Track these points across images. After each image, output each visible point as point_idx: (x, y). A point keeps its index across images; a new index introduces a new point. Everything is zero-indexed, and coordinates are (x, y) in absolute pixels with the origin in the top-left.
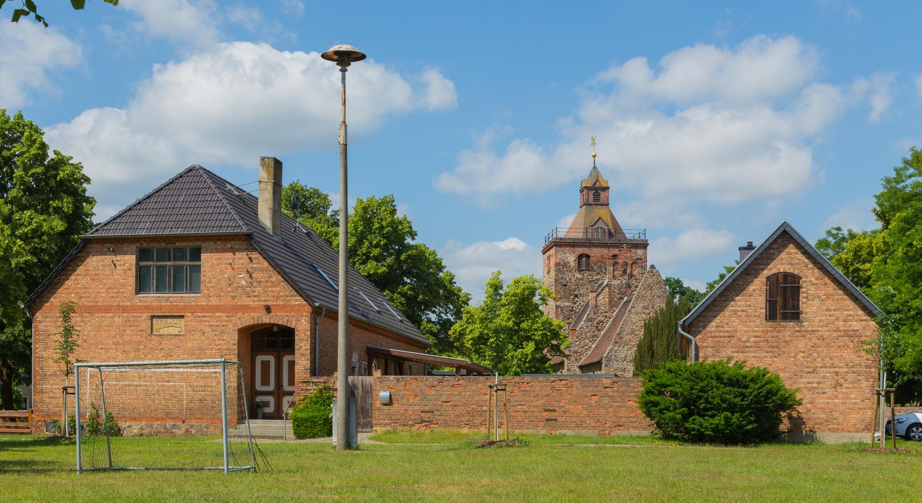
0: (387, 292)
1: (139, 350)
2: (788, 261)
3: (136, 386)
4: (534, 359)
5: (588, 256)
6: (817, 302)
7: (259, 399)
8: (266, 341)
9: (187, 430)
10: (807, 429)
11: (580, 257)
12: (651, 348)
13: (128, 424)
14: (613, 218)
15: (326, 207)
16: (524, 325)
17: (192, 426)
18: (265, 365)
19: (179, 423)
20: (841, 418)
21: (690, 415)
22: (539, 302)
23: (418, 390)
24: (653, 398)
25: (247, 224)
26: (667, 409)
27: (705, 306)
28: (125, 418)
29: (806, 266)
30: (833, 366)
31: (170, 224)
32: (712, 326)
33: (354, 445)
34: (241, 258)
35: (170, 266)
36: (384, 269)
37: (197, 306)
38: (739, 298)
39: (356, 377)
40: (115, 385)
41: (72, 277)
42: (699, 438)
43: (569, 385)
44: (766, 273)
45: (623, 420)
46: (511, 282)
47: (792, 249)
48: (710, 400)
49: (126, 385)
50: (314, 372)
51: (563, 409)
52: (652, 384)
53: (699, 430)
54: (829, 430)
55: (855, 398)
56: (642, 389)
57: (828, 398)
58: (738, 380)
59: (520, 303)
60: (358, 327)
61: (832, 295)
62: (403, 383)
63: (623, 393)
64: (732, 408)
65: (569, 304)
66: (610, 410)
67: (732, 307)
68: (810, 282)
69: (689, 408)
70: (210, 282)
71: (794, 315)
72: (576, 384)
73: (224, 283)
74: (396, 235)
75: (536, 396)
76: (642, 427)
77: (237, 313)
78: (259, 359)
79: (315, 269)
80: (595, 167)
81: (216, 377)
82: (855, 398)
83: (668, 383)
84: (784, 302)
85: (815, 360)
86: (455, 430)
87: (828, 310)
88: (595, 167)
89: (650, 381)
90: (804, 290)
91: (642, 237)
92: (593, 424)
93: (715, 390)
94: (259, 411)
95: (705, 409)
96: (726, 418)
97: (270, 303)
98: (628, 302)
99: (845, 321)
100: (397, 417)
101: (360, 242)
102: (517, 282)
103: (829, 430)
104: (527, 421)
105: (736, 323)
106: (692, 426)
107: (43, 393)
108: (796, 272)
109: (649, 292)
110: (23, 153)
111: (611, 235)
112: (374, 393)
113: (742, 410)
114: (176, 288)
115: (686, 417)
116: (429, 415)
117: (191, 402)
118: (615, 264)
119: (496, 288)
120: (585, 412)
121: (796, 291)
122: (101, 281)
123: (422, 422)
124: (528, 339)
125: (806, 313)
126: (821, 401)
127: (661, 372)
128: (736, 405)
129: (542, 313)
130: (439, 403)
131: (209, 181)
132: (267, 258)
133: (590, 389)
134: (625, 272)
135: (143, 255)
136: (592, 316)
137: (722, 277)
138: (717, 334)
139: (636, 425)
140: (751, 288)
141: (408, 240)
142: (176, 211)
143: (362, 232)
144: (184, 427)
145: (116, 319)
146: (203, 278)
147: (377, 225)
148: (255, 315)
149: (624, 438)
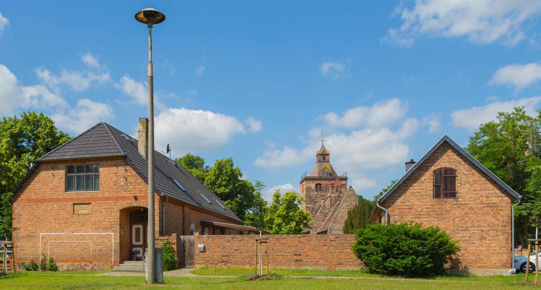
1: (67, 223)
2: (448, 160)
3: (66, 243)
4: (295, 230)
5: (320, 184)
6: (467, 186)
7: (134, 249)
8: (135, 216)
9: (92, 267)
10: (463, 266)
11: (317, 185)
12: (351, 223)
13: (61, 264)
14: (331, 167)
15: (202, 164)
16: (291, 214)
17: (95, 265)
18: (138, 230)
19: (88, 264)
20: (486, 259)
21: (388, 257)
22: (298, 203)
23: (220, 243)
24: (362, 247)
25: (124, 151)
26: (372, 254)
27: (394, 190)
28: (60, 261)
29: (460, 163)
30: (479, 226)
31: (83, 152)
32: (398, 202)
33: (160, 280)
34: (121, 170)
35: (83, 176)
36: (228, 190)
37: (98, 197)
38: (415, 184)
39: (185, 236)
40: (55, 243)
41: (32, 183)
42: (393, 273)
43: (309, 239)
44: (433, 168)
45: (342, 260)
46: (284, 194)
47: (450, 153)
48: (401, 248)
49: (60, 242)
50: (161, 234)
51: (306, 254)
52: (361, 238)
53: (394, 267)
54: (478, 267)
55: (495, 247)
56: (356, 241)
57: (476, 246)
58: (419, 235)
59: (289, 204)
60: (194, 210)
61: (478, 181)
62: (211, 239)
63: (343, 244)
64: (417, 253)
66: (335, 254)
67: (411, 190)
68: (463, 173)
69: (387, 253)
70: (104, 184)
71: (453, 194)
72: (313, 239)
73: (112, 184)
74: (233, 176)
75: (290, 246)
76: (356, 265)
77: (119, 201)
78: (134, 227)
79: (171, 179)
81: (108, 237)
82: (495, 247)
83: (373, 237)
84: (445, 186)
85: (467, 222)
86: (241, 267)
87: (475, 190)
89: (360, 236)
90: (458, 178)
91: (345, 176)
92: (324, 263)
93: (404, 241)
94: (134, 256)
95: (397, 254)
96: (412, 260)
97: (137, 195)
98: (339, 204)
99: (487, 197)
100: (208, 259)
101: (217, 179)
102: (287, 194)
103: (478, 267)
104: (284, 261)
105: (414, 200)
106: (390, 265)
107: (17, 247)
108: (453, 167)
109: (349, 198)
110: (42, 132)
111: (330, 175)
112: (195, 245)
113: (423, 254)
114: (87, 188)
115: (385, 259)
116: (226, 258)
117: (95, 251)
118: (333, 187)
119: (277, 197)
120: (319, 256)
121: (453, 179)
122: (47, 185)
123: (223, 262)
124: (293, 220)
125: (460, 193)
126: (471, 248)
127: (366, 231)
128: (418, 251)
129: (299, 208)
130: (232, 251)
131: (108, 130)
132: (135, 169)
133: (322, 241)
134: (337, 190)
135: (70, 170)
137: (385, 191)
138: (402, 207)
139: (351, 263)
140: (423, 178)
141: (239, 178)
142: (88, 146)
143: (218, 174)
144: (91, 265)
145: (55, 206)
146: (100, 182)
147: (225, 171)
148: (129, 202)
149: (344, 272)
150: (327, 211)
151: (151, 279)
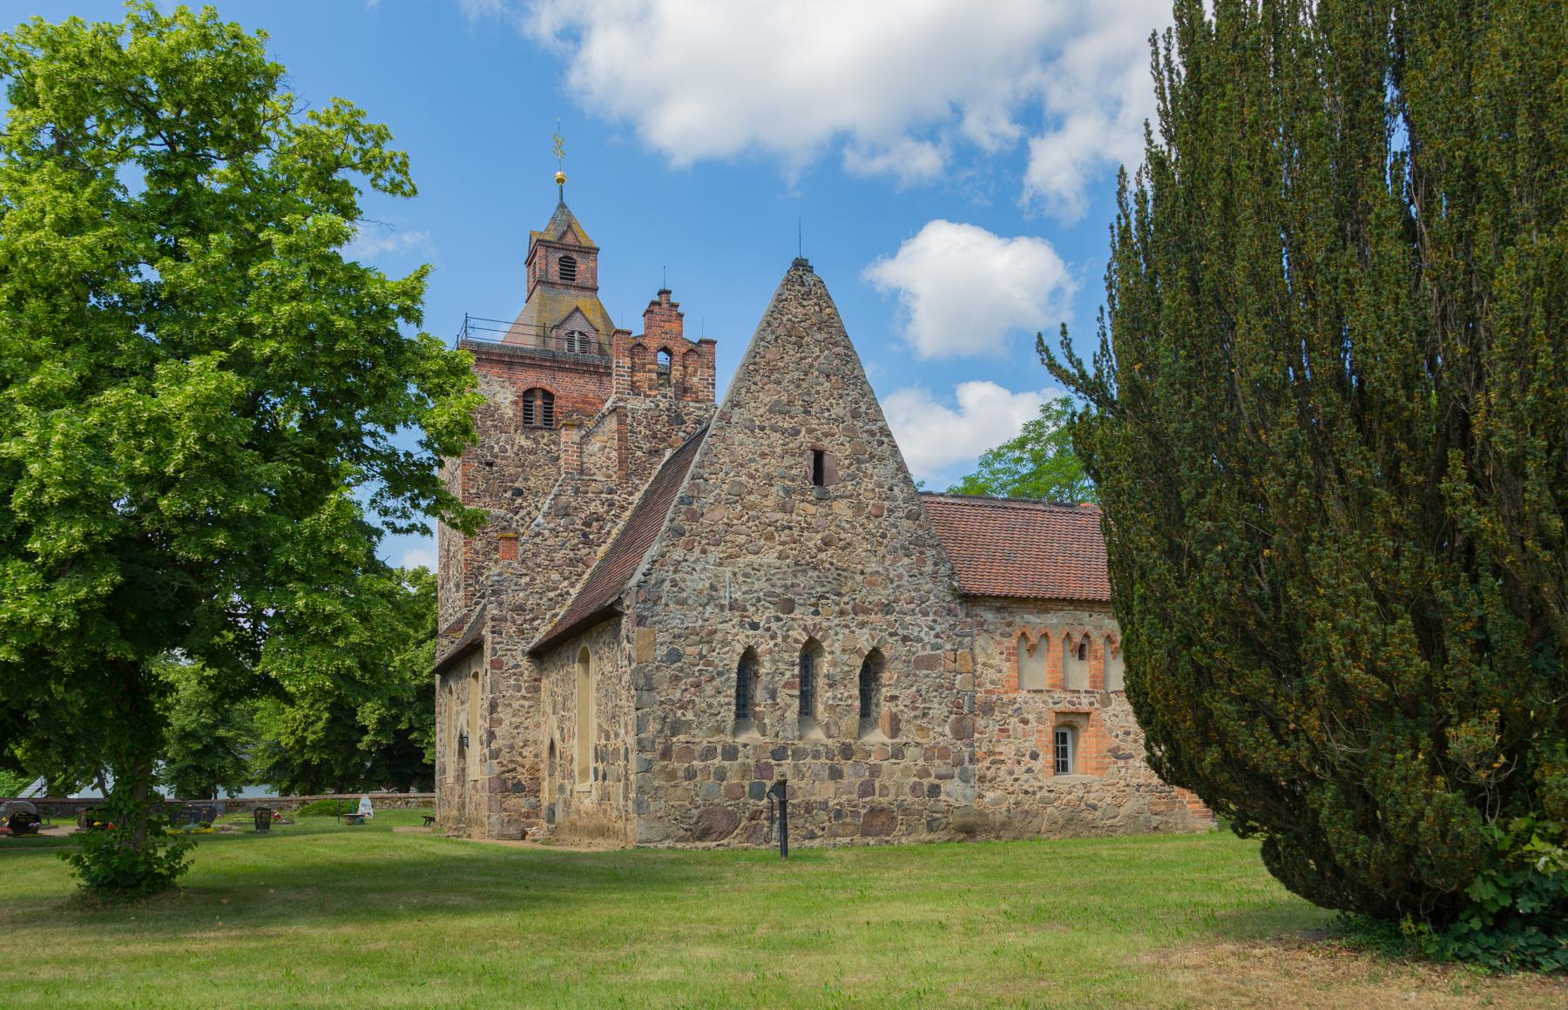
0: (413, 792)
5: (548, 396)
11: (529, 394)
65: (502, 512)
80: (562, 206)
88: (562, 206)
136: (567, 498)
150: (596, 507)
151: (318, 860)
